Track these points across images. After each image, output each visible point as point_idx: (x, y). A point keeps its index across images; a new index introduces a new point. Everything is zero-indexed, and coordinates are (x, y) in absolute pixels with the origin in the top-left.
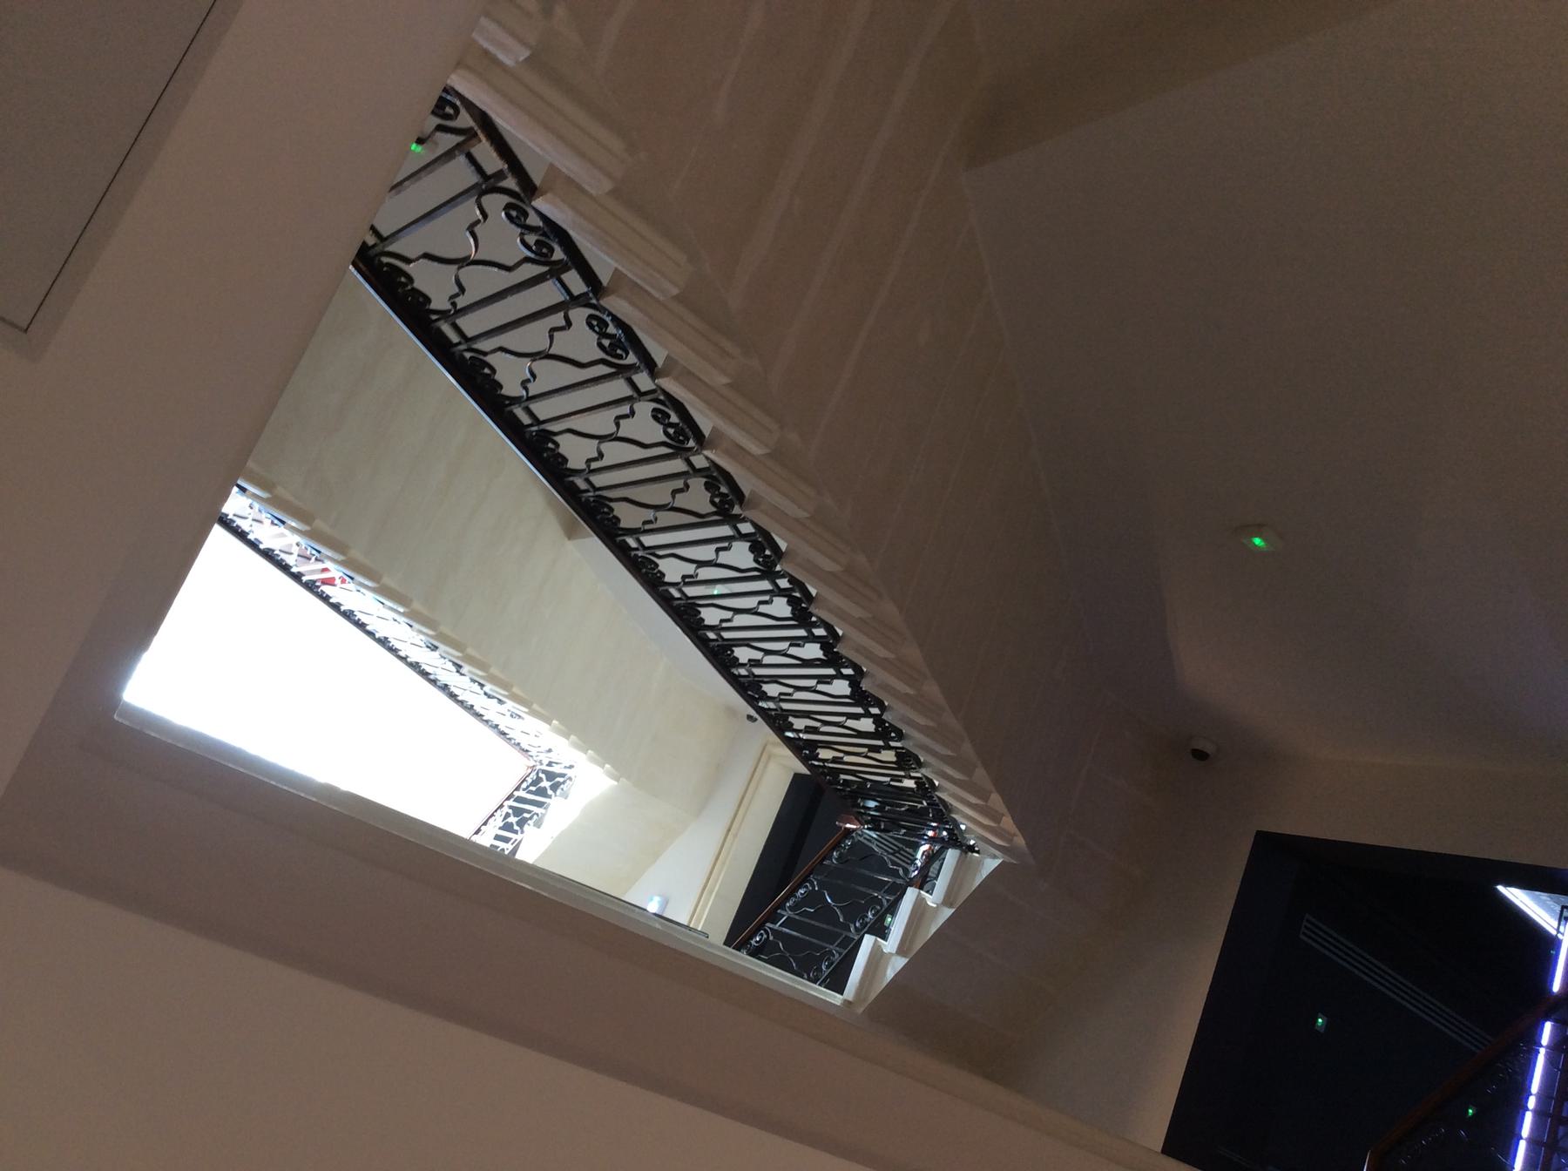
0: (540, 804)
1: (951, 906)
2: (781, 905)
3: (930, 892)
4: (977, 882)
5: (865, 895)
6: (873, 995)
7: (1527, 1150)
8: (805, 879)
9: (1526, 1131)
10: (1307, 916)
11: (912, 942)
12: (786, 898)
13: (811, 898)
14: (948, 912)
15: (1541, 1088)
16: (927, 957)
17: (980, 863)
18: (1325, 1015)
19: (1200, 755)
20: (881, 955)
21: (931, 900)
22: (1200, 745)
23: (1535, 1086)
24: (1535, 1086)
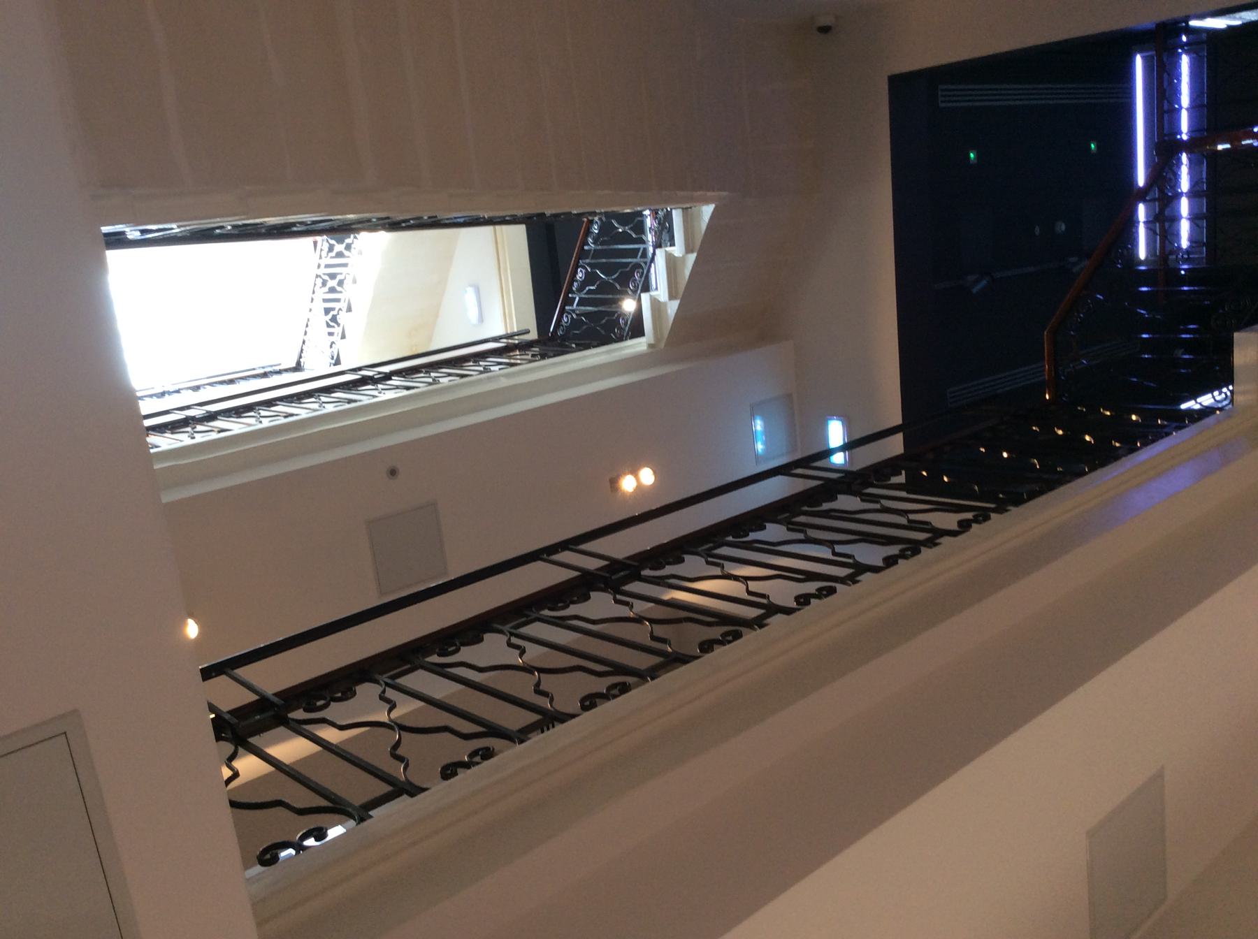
0: (345, 265)
1: (692, 252)
2: (570, 290)
3: (673, 244)
4: (704, 226)
5: (627, 264)
6: (666, 333)
7: (1191, 173)
8: (577, 266)
9: (1184, 116)
10: (941, 87)
11: (676, 287)
12: (571, 284)
13: (590, 278)
14: (692, 257)
15: (1190, 126)
16: (689, 293)
17: (700, 214)
18: (972, 149)
19: (825, 30)
20: (655, 299)
21: (677, 250)
22: (824, 21)
23: (1185, 100)
24: (1185, 100)
